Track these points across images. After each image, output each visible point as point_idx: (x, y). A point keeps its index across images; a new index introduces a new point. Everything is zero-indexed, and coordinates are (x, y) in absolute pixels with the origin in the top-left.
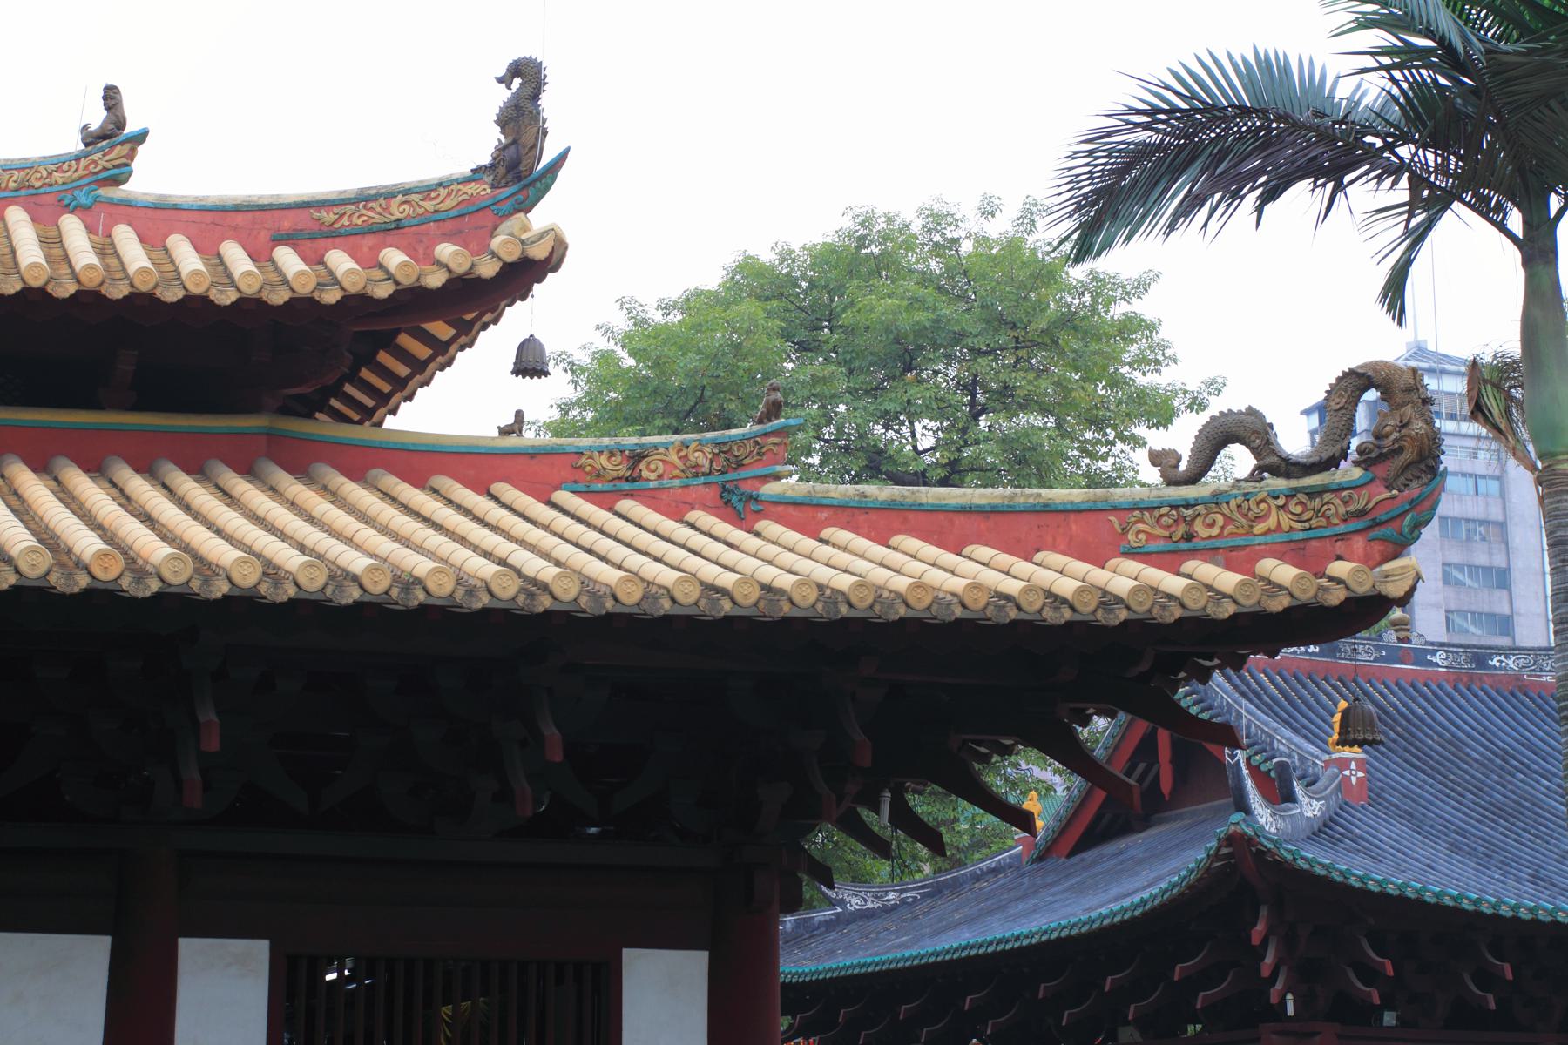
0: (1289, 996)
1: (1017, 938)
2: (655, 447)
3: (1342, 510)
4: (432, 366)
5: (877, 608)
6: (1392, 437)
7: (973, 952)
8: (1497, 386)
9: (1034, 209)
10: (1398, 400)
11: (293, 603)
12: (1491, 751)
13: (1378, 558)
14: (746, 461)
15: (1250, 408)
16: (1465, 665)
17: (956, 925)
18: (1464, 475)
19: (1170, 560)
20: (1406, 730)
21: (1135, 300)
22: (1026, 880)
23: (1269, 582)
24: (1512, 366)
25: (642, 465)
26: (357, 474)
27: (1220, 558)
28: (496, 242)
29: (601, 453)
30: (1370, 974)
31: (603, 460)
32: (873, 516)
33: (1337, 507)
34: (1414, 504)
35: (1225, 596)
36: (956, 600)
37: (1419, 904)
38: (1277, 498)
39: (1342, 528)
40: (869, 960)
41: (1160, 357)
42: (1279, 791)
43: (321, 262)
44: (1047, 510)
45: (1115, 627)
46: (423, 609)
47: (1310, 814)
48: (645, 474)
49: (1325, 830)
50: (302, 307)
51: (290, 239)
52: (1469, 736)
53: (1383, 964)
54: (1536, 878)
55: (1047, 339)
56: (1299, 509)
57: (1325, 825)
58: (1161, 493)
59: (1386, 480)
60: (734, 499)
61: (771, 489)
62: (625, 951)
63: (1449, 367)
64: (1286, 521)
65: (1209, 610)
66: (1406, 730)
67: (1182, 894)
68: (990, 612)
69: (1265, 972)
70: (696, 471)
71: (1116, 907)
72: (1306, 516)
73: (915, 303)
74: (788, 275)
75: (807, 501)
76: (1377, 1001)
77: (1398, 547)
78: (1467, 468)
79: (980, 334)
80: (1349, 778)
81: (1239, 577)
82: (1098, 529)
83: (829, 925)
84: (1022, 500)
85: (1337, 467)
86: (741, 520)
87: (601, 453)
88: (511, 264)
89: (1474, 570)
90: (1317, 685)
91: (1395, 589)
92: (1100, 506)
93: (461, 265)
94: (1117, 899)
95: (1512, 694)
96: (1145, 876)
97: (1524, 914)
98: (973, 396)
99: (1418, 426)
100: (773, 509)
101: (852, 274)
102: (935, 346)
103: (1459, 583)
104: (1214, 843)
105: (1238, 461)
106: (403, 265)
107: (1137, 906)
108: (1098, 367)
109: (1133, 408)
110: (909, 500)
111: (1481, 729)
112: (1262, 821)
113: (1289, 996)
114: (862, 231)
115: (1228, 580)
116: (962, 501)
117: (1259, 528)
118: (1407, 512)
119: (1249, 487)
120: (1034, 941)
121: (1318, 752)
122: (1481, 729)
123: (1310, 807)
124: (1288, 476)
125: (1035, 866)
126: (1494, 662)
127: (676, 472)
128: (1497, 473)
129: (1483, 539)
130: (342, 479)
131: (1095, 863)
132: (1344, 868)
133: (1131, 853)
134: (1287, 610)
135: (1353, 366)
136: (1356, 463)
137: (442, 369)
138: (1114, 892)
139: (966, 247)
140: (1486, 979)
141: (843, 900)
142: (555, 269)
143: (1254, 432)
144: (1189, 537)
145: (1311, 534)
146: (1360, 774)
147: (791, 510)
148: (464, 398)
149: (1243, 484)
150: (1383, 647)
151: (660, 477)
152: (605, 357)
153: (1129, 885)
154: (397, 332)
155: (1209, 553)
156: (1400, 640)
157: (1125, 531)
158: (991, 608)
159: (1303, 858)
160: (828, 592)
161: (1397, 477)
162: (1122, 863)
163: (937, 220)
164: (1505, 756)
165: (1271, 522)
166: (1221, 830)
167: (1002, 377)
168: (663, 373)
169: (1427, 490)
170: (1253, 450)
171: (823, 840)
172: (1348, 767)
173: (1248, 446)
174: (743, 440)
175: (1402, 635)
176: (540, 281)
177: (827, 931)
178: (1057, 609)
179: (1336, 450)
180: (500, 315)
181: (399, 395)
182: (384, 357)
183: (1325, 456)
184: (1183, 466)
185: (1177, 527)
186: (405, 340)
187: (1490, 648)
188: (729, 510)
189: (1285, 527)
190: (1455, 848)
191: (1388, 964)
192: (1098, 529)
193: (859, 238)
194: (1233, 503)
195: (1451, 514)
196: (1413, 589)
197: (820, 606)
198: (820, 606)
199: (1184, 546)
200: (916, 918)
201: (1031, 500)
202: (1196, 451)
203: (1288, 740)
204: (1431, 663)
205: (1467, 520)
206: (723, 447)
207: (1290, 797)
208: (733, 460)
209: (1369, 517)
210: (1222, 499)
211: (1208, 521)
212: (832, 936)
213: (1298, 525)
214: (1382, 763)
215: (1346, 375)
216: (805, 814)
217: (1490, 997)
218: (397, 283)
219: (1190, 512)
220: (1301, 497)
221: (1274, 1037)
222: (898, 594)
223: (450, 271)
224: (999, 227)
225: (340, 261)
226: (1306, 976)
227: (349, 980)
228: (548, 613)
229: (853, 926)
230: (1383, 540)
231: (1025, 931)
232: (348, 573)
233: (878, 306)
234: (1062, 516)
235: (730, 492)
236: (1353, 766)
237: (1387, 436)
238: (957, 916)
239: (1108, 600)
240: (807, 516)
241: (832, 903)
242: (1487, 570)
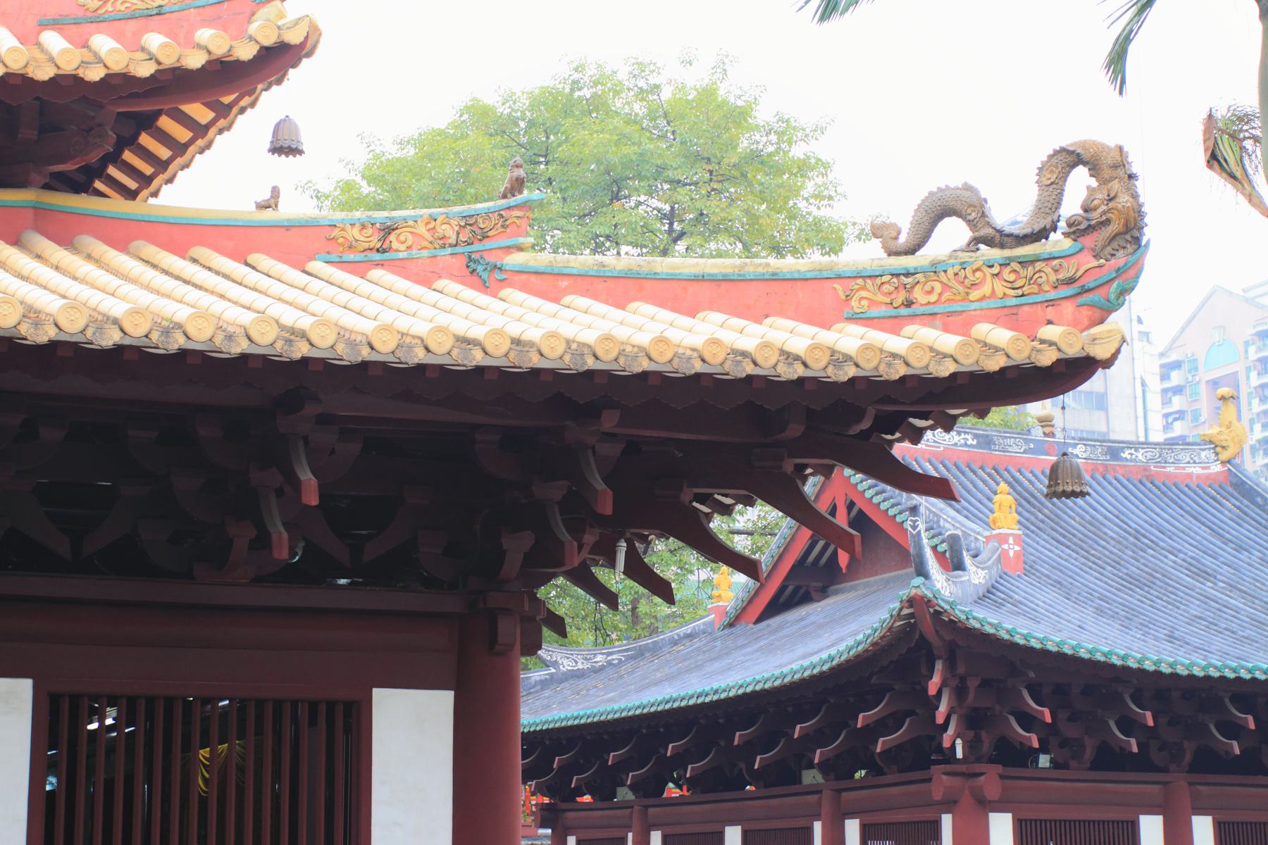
0: (959, 741)
1: (716, 692)
2: (405, 220)
3: (1053, 278)
4: (192, 149)
5: (622, 360)
6: (1100, 210)
7: (676, 705)
8: (1233, 136)
9: (726, 60)
10: (1106, 176)
11: (53, 345)
12: (1125, 531)
13: (1086, 322)
14: (490, 234)
15: (966, 184)
16: (1099, 454)
17: (656, 683)
19: (893, 324)
20: (1051, 512)
21: (813, 141)
22: (718, 643)
23: (986, 344)
24: (1244, 118)
25: (392, 237)
26: (121, 245)
27: (938, 323)
28: (253, 28)
29: (353, 225)
30: (1028, 721)
31: (355, 232)
32: (611, 284)
33: (1048, 275)
34: (1120, 272)
35: (945, 356)
36: (695, 354)
37: (1074, 660)
38: (991, 266)
39: (1053, 295)
40: (582, 713)
41: (833, 194)
42: (953, 563)
43: (85, 45)
44: (775, 278)
45: (843, 383)
46: (183, 354)
47: (976, 582)
48: (395, 245)
49: (988, 595)
50: (66, 85)
51: (55, 24)
52: (1105, 517)
53: (1042, 712)
54: (1171, 638)
55: (739, 174)
56: (1012, 277)
57: (988, 592)
58: (882, 263)
59: (1093, 250)
60: (480, 268)
61: (515, 260)
62: (375, 691)
64: (1000, 288)
65: (931, 369)
66: (1051, 512)
67: (866, 651)
68: (728, 367)
69: (940, 720)
70: (443, 242)
71: (806, 663)
72: (1018, 284)
73: (623, 139)
74: (510, 115)
75: (549, 270)
76: (1036, 745)
77: (1103, 313)
79: (680, 167)
80: (1007, 551)
81: (958, 339)
82: (821, 296)
83: (544, 684)
84: (751, 269)
85: (1047, 238)
86: (484, 287)
87: (353, 225)
88: (267, 49)
90: (975, 473)
91: (1101, 352)
92: (825, 275)
93: (219, 50)
94: (804, 657)
95: (1141, 482)
96: (827, 637)
97: (1165, 669)
98: (671, 224)
99: (1124, 200)
100: (517, 278)
101: (566, 113)
102: (640, 177)
104: (897, 605)
105: (951, 235)
106: (164, 46)
107: (825, 662)
108: (779, 200)
109: (811, 234)
110: (645, 270)
111: (1116, 512)
112: (938, 585)
113: (959, 741)
114: (576, 76)
115: (949, 342)
116: (697, 271)
117: (975, 294)
118: (1112, 280)
119: (965, 256)
120: (731, 694)
121: (980, 529)
122: (1116, 512)
123: (976, 576)
124: (1002, 246)
125: (726, 631)
126: (1126, 455)
127: (425, 244)
130: (106, 248)
131: (780, 628)
132: (1010, 627)
133: (812, 618)
134: (1003, 370)
135: (1064, 145)
136: (1066, 235)
137: (202, 151)
138: (801, 650)
139: (666, 94)
140: (1129, 725)
141: (556, 662)
142: (309, 55)
143: (970, 206)
144: (909, 304)
145: (1023, 300)
146: (1017, 548)
147: (533, 278)
148: (219, 175)
149: (959, 254)
150: (1032, 441)
151: (409, 248)
152: (348, 187)
153: (813, 645)
154: (158, 114)
155: (929, 318)
157: (848, 298)
158: (728, 363)
159: (974, 618)
160: (574, 346)
161: (1104, 247)
162: (804, 627)
163: (641, 68)
164: (1137, 535)
165: (986, 290)
166: (904, 593)
167: (699, 205)
168: (399, 197)
169: (1132, 259)
170: (969, 222)
171: (560, 595)
172: (1006, 542)
173: (964, 219)
174: (488, 214)
175: (1048, 430)
176: (294, 66)
177: (542, 689)
178: (790, 364)
179: (1047, 222)
180: (257, 99)
181: (161, 177)
182: (145, 140)
183: (1037, 228)
184: (902, 239)
185: (901, 297)
186: (165, 123)
187: (1122, 442)
188: (475, 278)
189: (999, 293)
190: (1100, 611)
191: (1046, 711)
192: (821, 296)
193: (574, 82)
194: (950, 272)
196: (1118, 351)
197: (567, 358)
198: (567, 358)
199: (904, 311)
200: (621, 677)
201: (760, 270)
202: (916, 224)
203: (953, 518)
206: (469, 221)
207: (959, 566)
208: (478, 231)
209: (1077, 285)
210: (940, 268)
211: (928, 288)
212: (547, 693)
213: (1012, 292)
214: (1033, 540)
215: (1056, 153)
216: (545, 562)
217: (1133, 741)
218: (159, 63)
219: (910, 280)
220: (1015, 265)
221: (944, 777)
222: (641, 348)
223: (209, 53)
224: (695, 78)
225: (103, 43)
226: (974, 722)
227: (111, 728)
228: (305, 361)
229: (566, 685)
230: (1091, 306)
231: (723, 686)
232: (108, 319)
233: (589, 143)
234: (789, 284)
235: (475, 262)
236: (1011, 540)
237: (1095, 209)
238: (659, 675)
239: (839, 359)
240: (549, 284)
241: (547, 665)
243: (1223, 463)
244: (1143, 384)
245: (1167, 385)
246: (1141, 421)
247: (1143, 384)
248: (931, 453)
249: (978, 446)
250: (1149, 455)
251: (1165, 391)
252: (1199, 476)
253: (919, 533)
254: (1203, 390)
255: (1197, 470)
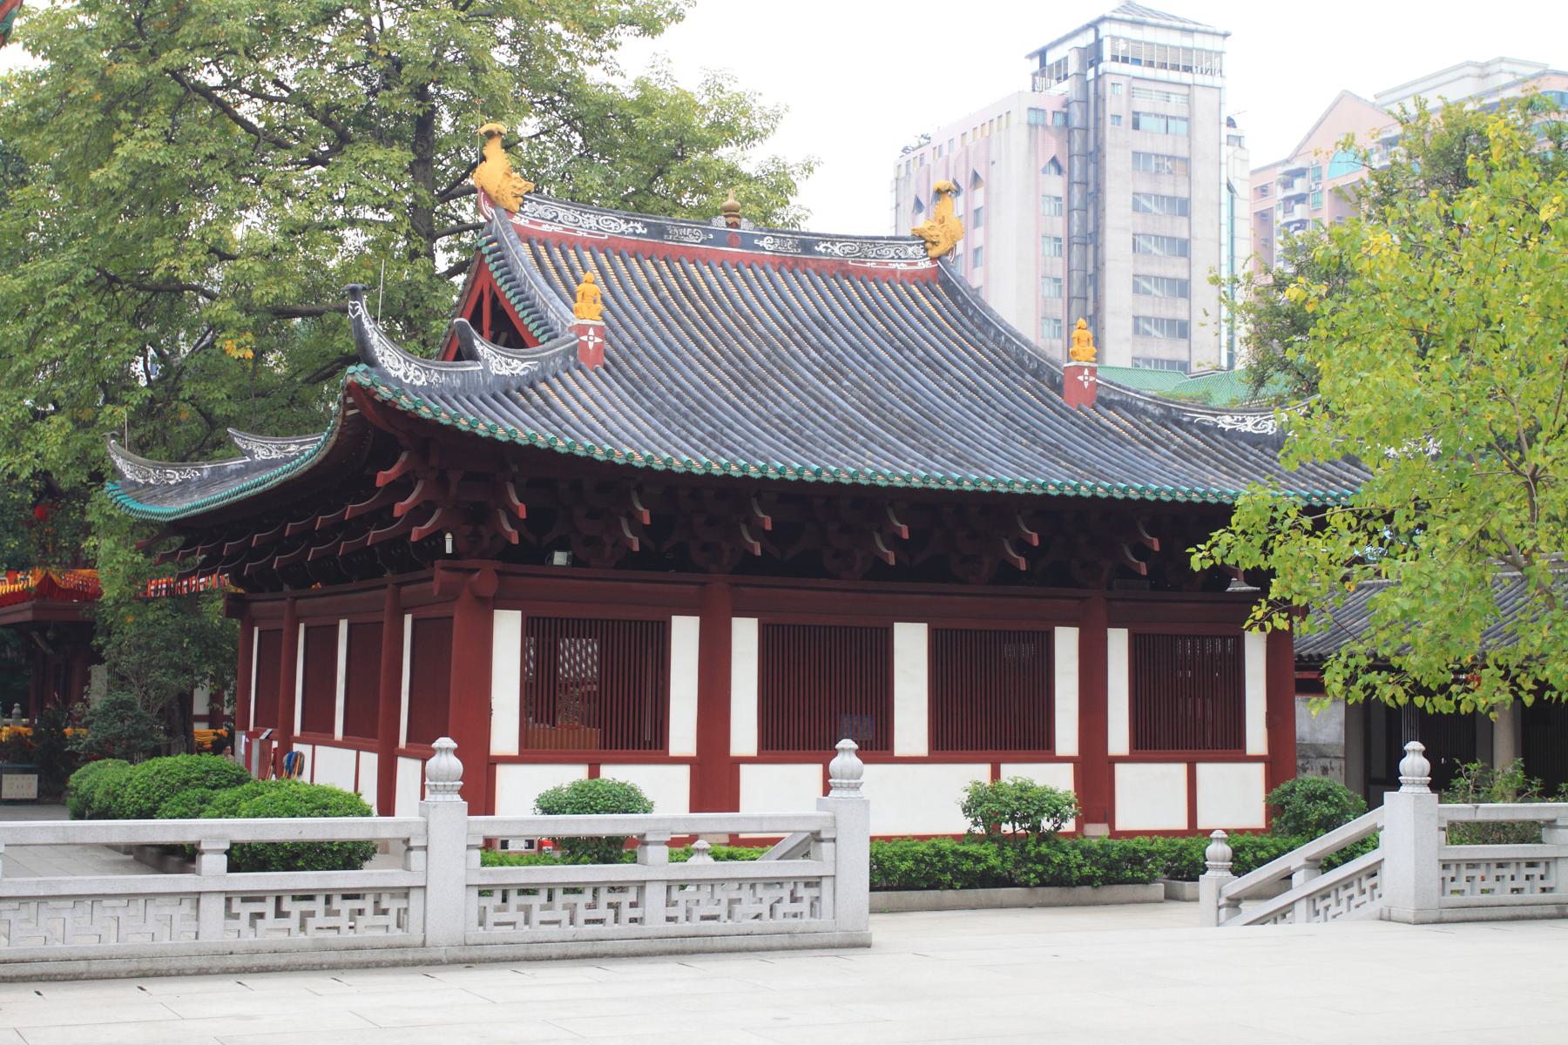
16: (790, 248)
18: (1157, 116)
63: (1149, 20)
78: (1161, 110)
89: (1160, 198)
103: (1146, 210)
126: (821, 248)
128: (1185, 114)
129: (1170, 172)
146: (598, 340)
156: (728, 225)
172: (586, 333)
175: (731, 220)
195: (1143, 150)
204: (757, 247)
205: (1157, 156)
236: (591, 332)
241: (244, 453)
242: (1172, 199)
243: (933, 259)
244: (1230, 188)
245: (1290, 193)
246: (1225, 230)
247: (1230, 188)
248: (593, 241)
249: (648, 235)
250: (847, 250)
251: (1288, 199)
252: (903, 273)
253: (359, 317)
254: (1326, 199)
255: (902, 266)
